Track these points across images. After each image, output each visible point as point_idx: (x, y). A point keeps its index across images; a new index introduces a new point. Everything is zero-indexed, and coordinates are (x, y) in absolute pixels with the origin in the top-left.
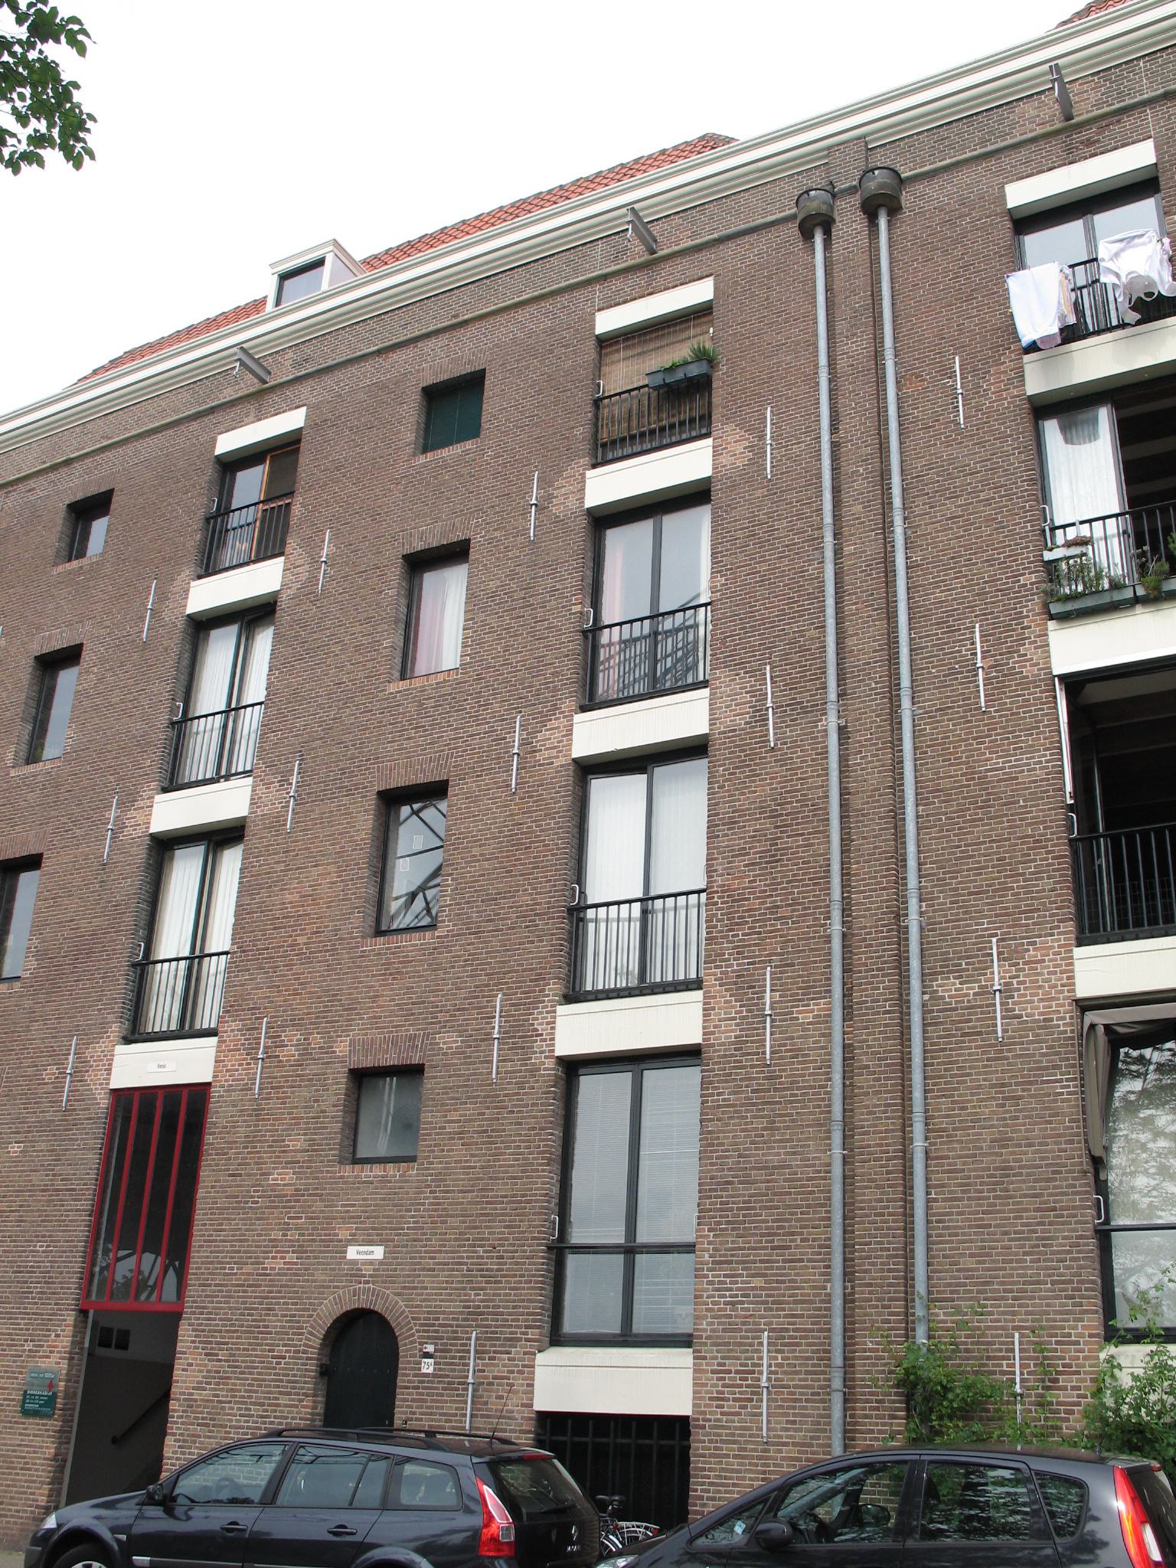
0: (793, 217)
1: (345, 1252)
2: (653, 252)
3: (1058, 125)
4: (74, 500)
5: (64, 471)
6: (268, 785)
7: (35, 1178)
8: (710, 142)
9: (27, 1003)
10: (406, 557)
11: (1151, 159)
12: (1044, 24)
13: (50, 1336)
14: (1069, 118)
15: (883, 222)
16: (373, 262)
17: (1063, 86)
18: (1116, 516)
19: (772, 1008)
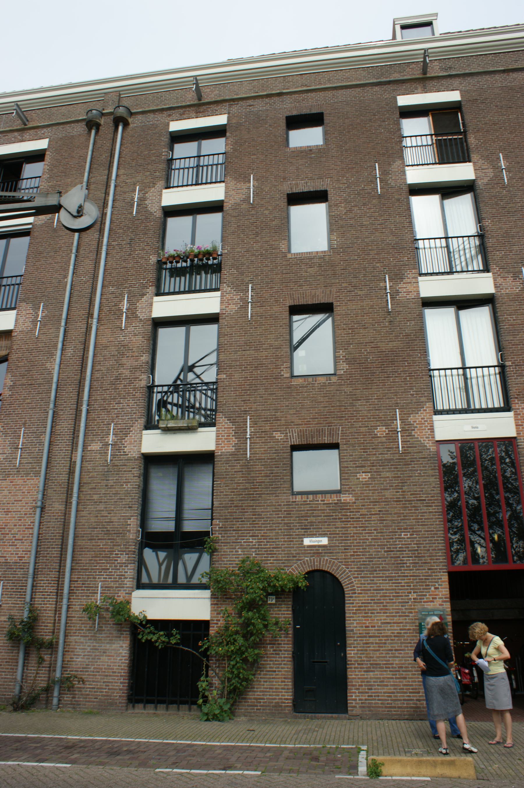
1: (303, 541)
2: (26, 125)
4: (290, 114)
5: (276, 99)
6: (505, 278)
7: (388, 494)
9: (348, 389)
10: (288, 195)
13: (430, 589)
15: (120, 128)
19: (22, 445)
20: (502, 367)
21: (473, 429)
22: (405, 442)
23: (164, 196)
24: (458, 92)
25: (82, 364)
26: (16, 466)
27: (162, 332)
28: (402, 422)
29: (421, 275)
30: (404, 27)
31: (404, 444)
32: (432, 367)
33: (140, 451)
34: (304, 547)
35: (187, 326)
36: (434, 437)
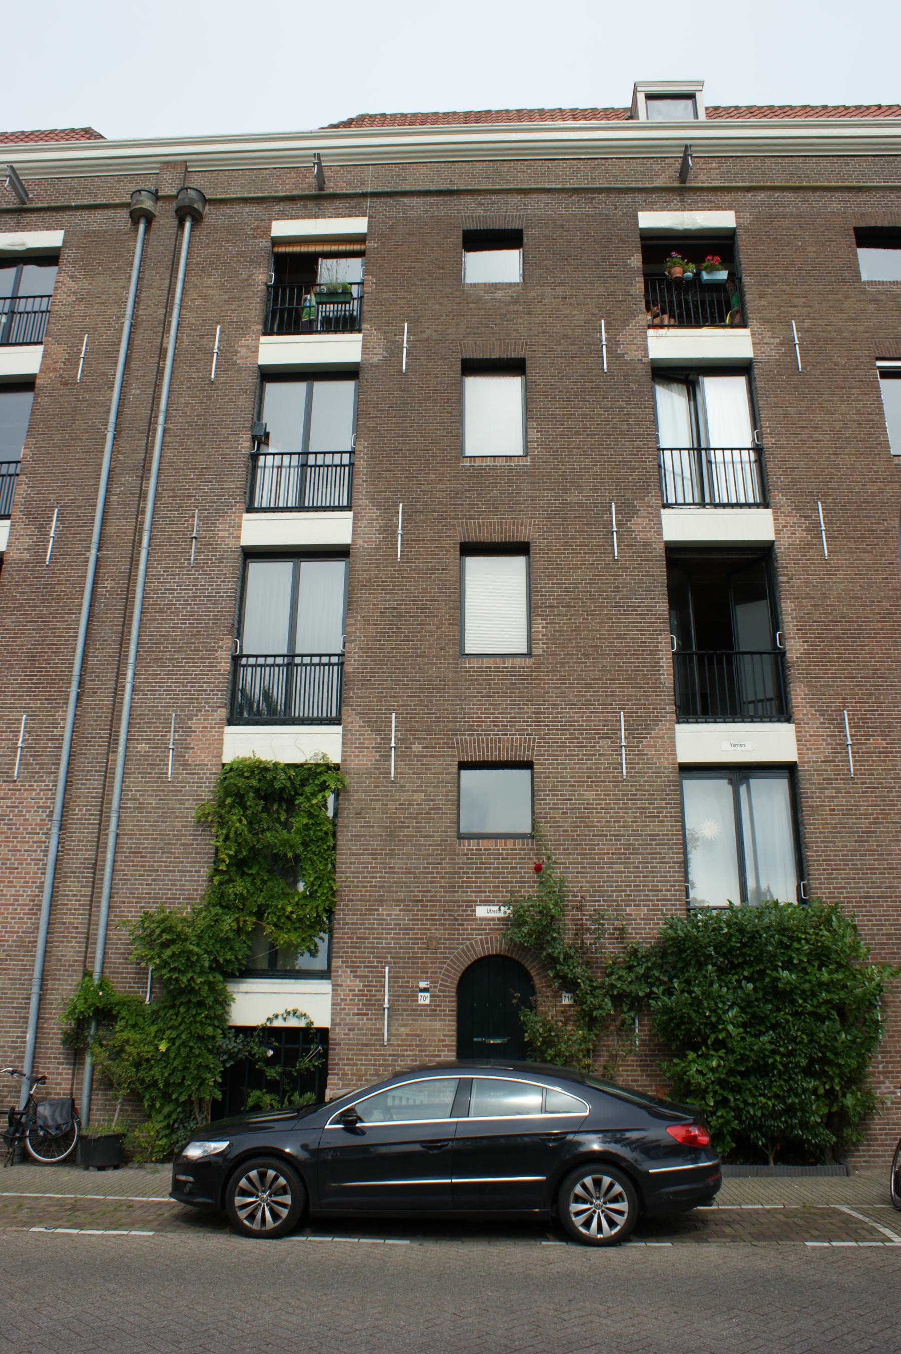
0: (128, 205)
1: (474, 911)
3: (314, 192)
8: (89, 133)
11: (59, 243)
12: (313, 124)
14: (321, 188)
15: (188, 225)
16: (714, 111)
17: (320, 168)
18: (299, 454)
20: (758, 449)
21: (733, 748)
22: (632, 763)
23: (227, 738)
24: (732, 214)
25: (122, 638)
26: (12, 777)
27: (255, 569)
28: (629, 734)
29: (666, 506)
30: (650, 97)
31: (631, 768)
32: (662, 446)
33: (221, 760)
34: (476, 920)
35: (310, 382)
36: (676, 759)
